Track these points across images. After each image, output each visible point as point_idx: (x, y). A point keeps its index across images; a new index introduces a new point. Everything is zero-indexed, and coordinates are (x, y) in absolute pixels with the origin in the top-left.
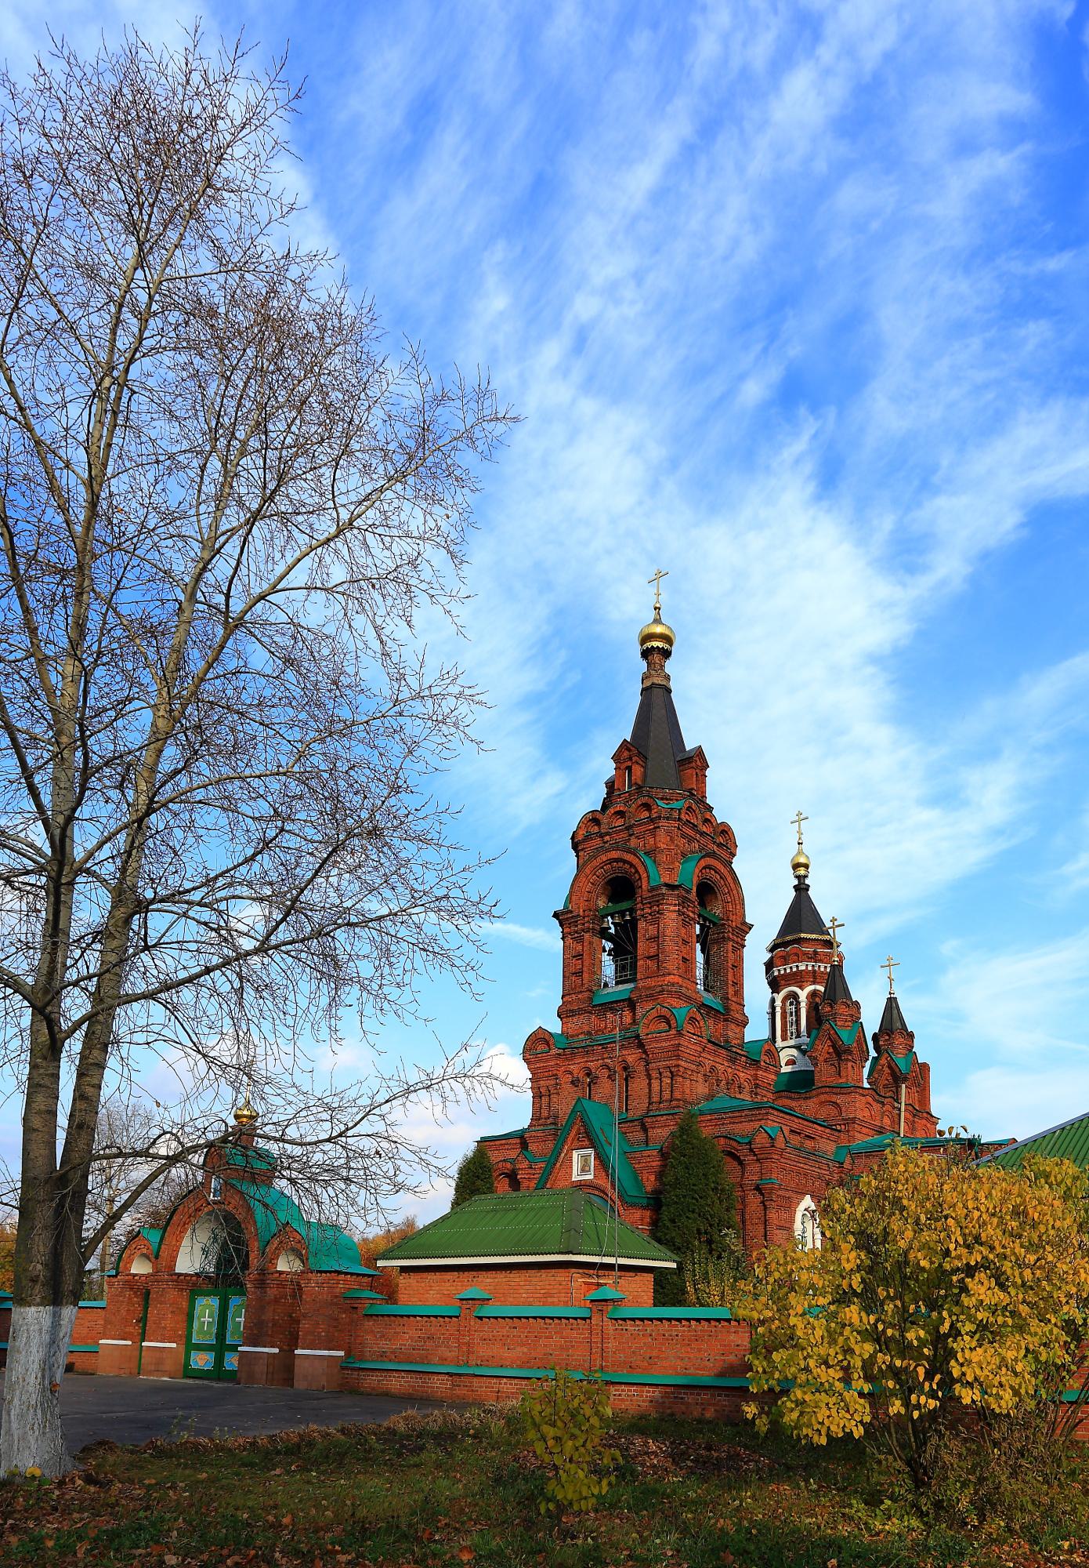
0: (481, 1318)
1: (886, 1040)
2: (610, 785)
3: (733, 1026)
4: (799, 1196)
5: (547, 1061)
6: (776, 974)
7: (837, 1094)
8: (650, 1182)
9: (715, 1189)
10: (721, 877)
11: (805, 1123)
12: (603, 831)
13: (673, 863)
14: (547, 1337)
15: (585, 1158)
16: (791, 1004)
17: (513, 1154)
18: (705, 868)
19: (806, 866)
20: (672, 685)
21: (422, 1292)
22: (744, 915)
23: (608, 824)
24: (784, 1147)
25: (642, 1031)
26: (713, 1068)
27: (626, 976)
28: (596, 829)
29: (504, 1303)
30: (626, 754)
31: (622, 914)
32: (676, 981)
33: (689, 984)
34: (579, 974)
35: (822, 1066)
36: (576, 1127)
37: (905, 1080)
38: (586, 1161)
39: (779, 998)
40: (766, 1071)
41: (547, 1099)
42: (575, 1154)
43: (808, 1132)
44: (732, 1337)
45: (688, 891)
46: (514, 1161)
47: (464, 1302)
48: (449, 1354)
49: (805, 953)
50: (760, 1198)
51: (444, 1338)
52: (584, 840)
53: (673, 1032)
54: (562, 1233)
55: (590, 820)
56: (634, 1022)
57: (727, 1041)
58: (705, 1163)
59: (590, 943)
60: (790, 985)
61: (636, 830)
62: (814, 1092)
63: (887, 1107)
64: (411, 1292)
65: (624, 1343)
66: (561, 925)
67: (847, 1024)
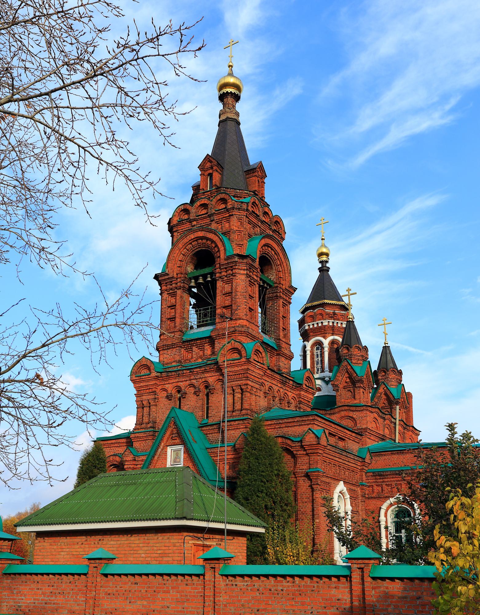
0: (106, 575)
1: (383, 376)
2: (196, 188)
3: (283, 359)
4: (336, 482)
5: (148, 381)
6: (307, 328)
7: (353, 411)
8: (226, 471)
9: (278, 475)
10: (275, 253)
11: (339, 428)
12: (191, 218)
13: (242, 240)
14: (164, 592)
15: (177, 452)
16: (317, 349)
17: (121, 450)
18: (265, 245)
19: (327, 255)
20: (241, 119)
21: (54, 553)
22: (291, 281)
23: (196, 212)
24: (326, 445)
25: (220, 359)
26: (270, 388)
27: (206, 321)
28: (186, 217)
29: (125, 562)
30: (209, 165)
31: (205, 276)
32: (244, 324)
33: (254, 327)
34: (172, 319)
35: (343, 392)
36: (170, 429)
37: (397, 403)
38: (177, 454)
39: (309, 345)
40: (306, 391)
41: (148, 409)
42: (169, 449)
43: (341, 434)
44: (334, 592)
45: (253, 260)
46: (121, 456)
47: (92, 561)
48: (77, 607)
49: (328, 314)
50: (308, 483)
51: (73, 593)
52: (177, 225)
53: (244, 360)
54: (176, 502)
55: (182, 210)
56: (213, 353)
57: (279, 370)
58: (270, 456)
59: (181, 297)
60: (316, 336)
61: (216, 218)
62: (337, 410)
63: (387, 422)
64: (45, 554)
65: (234, 597)
66: (160, 284)
67: (359, 362)
